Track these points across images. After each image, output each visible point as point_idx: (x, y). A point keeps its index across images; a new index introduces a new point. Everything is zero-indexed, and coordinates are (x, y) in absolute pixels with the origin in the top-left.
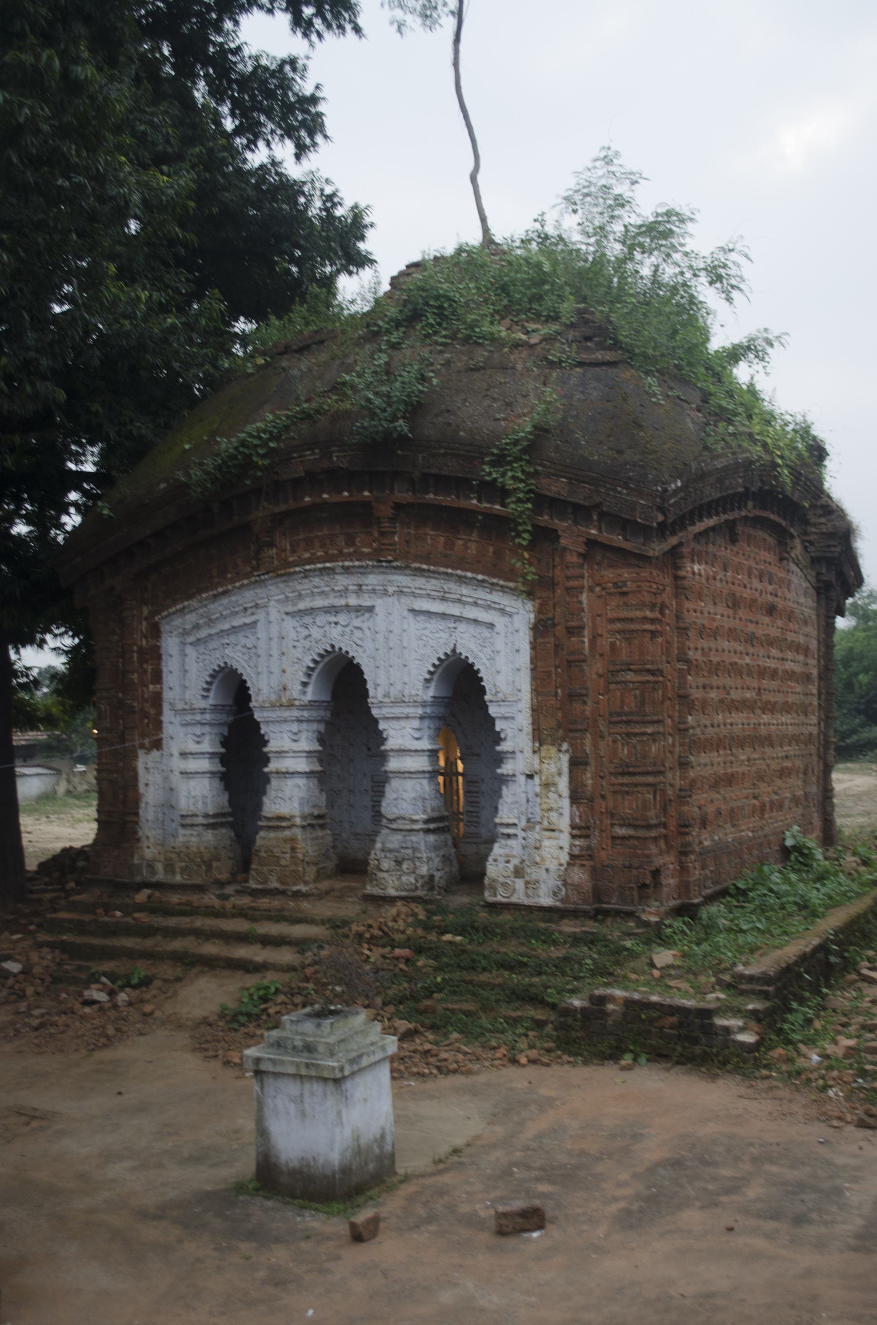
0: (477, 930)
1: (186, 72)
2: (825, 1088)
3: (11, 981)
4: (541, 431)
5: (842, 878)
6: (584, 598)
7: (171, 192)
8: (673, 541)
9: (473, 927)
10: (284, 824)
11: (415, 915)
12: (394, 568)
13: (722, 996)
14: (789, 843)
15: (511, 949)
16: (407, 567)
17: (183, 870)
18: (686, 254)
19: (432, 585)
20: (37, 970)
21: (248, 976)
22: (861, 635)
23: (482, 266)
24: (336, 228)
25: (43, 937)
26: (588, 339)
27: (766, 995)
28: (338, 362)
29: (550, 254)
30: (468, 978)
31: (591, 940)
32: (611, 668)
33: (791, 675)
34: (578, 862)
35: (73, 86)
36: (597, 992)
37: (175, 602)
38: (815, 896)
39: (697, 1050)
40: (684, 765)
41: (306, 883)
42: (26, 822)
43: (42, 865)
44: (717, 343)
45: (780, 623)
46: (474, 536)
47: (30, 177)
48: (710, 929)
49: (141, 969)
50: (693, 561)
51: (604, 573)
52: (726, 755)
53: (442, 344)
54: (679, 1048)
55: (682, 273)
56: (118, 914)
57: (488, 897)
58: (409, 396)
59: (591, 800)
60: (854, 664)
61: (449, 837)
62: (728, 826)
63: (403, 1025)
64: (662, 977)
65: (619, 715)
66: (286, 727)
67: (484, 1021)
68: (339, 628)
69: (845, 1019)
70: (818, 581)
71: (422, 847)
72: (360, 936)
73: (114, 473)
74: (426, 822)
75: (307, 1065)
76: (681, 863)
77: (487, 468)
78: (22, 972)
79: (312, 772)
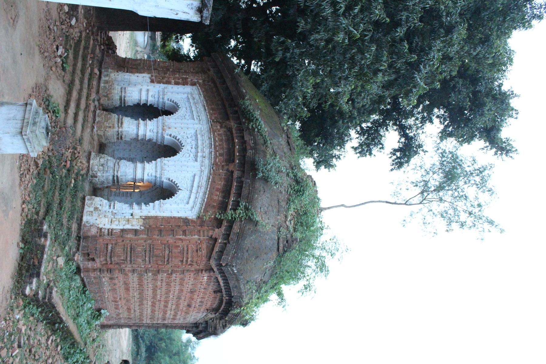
1: (381, 113)
2: (5, 320)
3: (68, 20)
4: (256, 223)
5: (88, 331)
6: (196, 237)
7: (342, 102)
8: (215, 269)
9: (76, 191)
10: (120, 124)
11: (82, 170)
12: (210, 170)
13: (45, 282)
14: (102, 311)
15: (67, 204)
17: (105, 87)
18: (314, 277)
19: (204, 183)
20: (71, 30)
21: (63, 107)
22: (180, 344)
23: (313, 206)
25: (84, 34)
26: (287, 242)
27: (44, 298)
28: (283, 155)
29: (317, 230)
30: (57, 188)
31: (69, 235)
32: (171, 245)
33: (165, 313)
35: (376, 72)
36: (49, 235)
37: (203, 92)
38: (81, 320)
39: (24, 272)
40: (133, 271)
41: (97, 131)
42: (127, 33)
43: (111, 37)
44: (284, 288)
45: (185, 309)
46: (220, 199)
47: (348, 56)
48: (71, 279)
49: (69, 68)
50: (208, 277)
52: (136, 288)
53: (288, 191)
54: (25, 265)
55: (308, 276)
56: (91, 62)
57: (87, 197)
58: (271, 178)
59: (122, 237)
62: (110, 288)
63: (40, 162)
64: (53, 260)
67: (40, 192)
68: (190, 149)
69: (33, 329)
70: (199, 324)
71: (108, 174)
72: (76, 149)
73: (250, 75)
74: (117, 176)
75: (28, 122)
76: (97, 269)
78: (71, 25)
79: (138, 136)
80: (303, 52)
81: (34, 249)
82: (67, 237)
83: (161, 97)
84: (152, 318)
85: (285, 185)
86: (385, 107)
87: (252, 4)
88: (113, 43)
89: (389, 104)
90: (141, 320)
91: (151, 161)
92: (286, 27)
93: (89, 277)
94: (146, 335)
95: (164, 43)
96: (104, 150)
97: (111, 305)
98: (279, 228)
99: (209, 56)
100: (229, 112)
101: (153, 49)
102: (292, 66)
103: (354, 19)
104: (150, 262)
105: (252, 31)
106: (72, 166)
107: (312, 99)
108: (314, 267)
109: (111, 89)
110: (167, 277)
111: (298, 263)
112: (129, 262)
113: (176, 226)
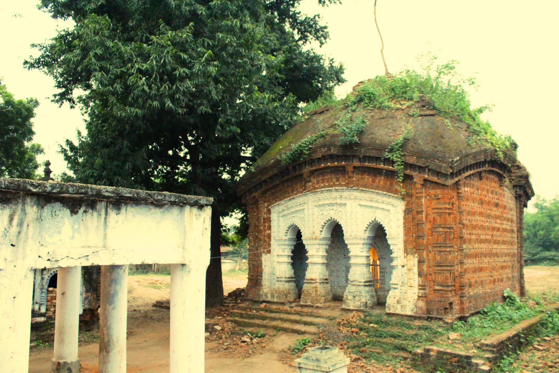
0: (382, 323)
1: (282, 21)
3: (217, 333)
4: (406, 140)
5: (527, 309)
6: (423, 200)
7: (276, 62)
8: (456, 179)
10: (313, 282)
11: (360, 316)
13: (475, 351)
14: (505, 295)
15: (395, 330)
16: (358, 189)
17: (277, 297)
20: (226, 329)
21: (299, 336)
23: (385, 82)
24: (334, 70)
25: (229, 318)
26: (424, 106)
27: (493, 352)
28: (333, 117)
31: (426, 329)
33: (505, 230)
34: (421, 299)
35: (243, 30)
36: (427, 347)
37: (276, 201)
38: (515, 315)
40: (462, 263)
41: (321, 303)
42: (224, 278)
43: (229, 294)
44: (472, 108)
45: (500, 210)
46: (382, 178)
47: (230, 60)
48: (472, 326)
49: (262, 331)
50: (465, 187)
51: (430, 191)
52: (479, 260)
56: (254, 311)
57: (387, 311)
58: (358, 128)
59: (426, 276)
60: (537, 227)
61: (372, 288)
64: (452, 343)
65: (436, 244)
66: (314, 246)
69: (527, 364)
70: (516, 194)
71: (363, 292)
72: (339, 323)
73: (256, 157)
74: (365, 282)
75: (317, 366)
77: (387, 153)
78: (221, 330)
80: (230, 106)
81: (441, 361)
82: (429, 331)
83: (284, 242)
84: (512, 243)
85: (364, 113)
86: (276, 17)
87: (187, 160)
88: (234, 292)
89: (272, 14)
90: (514, 255)
91: (348, 249)
92: (207, 124)
93: (469, 308)
94: (531, 251)
95: (230, 243)
96: (339, 296)
97: (498, 287)
98: (410, 116)
99: (240, 198)
100: (295, 175)
101: (236, 253)
102: (244, 115)
103: (106, 84)
104: (452, 247)
105: (213, 157)
106: (357, 326)
107: (275, 93)
108: (449, 76)
109: (279, 291)
110: (467, 229)
111: (446, 93)
112: (452, 268)
113: (413, 221)
